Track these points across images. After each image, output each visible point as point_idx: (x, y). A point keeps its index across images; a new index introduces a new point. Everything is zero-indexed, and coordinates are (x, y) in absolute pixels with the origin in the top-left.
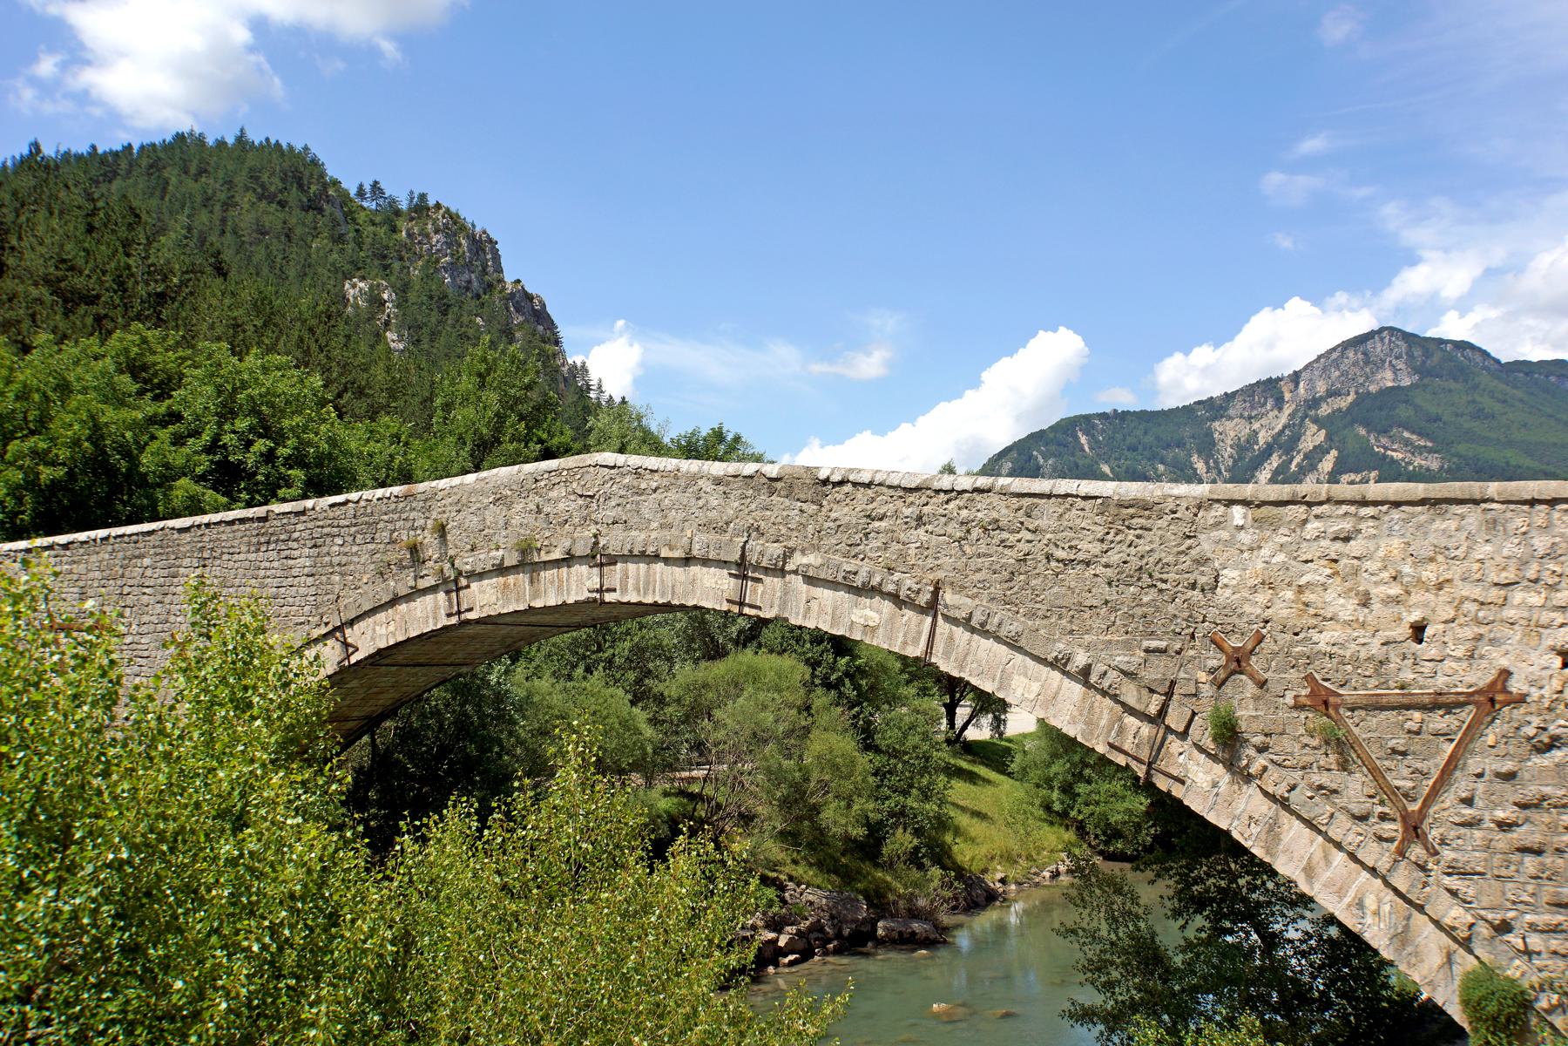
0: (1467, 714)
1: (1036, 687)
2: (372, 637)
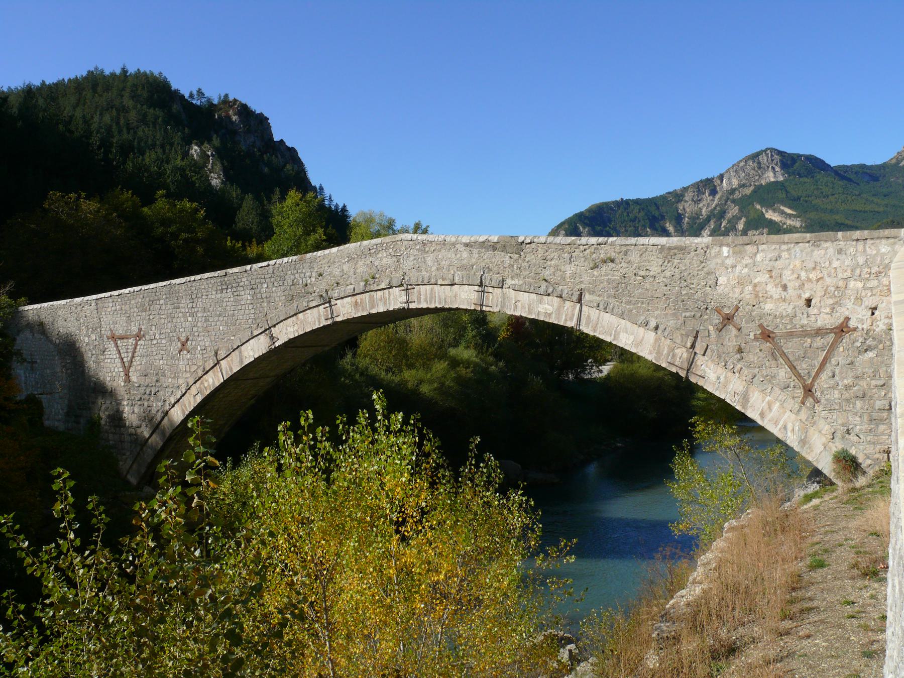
0: (831, 337)
1: (632, 338)
2: (286, 332)
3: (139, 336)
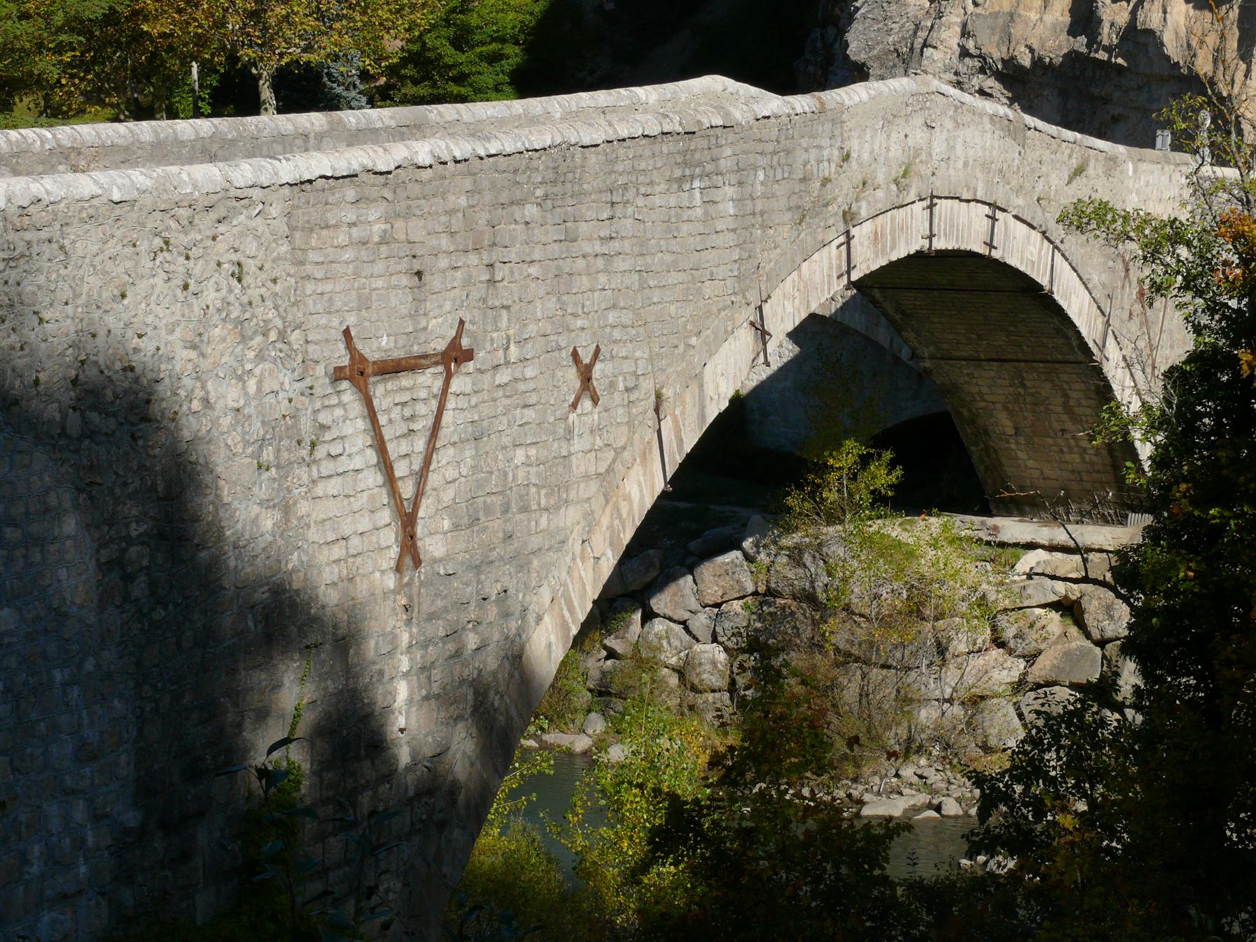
3: (456, 355)
